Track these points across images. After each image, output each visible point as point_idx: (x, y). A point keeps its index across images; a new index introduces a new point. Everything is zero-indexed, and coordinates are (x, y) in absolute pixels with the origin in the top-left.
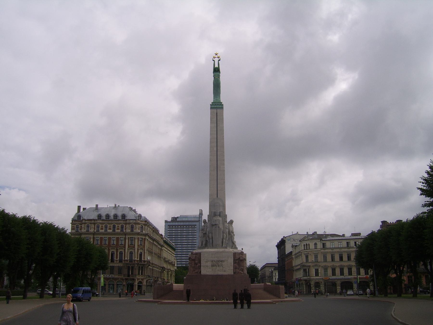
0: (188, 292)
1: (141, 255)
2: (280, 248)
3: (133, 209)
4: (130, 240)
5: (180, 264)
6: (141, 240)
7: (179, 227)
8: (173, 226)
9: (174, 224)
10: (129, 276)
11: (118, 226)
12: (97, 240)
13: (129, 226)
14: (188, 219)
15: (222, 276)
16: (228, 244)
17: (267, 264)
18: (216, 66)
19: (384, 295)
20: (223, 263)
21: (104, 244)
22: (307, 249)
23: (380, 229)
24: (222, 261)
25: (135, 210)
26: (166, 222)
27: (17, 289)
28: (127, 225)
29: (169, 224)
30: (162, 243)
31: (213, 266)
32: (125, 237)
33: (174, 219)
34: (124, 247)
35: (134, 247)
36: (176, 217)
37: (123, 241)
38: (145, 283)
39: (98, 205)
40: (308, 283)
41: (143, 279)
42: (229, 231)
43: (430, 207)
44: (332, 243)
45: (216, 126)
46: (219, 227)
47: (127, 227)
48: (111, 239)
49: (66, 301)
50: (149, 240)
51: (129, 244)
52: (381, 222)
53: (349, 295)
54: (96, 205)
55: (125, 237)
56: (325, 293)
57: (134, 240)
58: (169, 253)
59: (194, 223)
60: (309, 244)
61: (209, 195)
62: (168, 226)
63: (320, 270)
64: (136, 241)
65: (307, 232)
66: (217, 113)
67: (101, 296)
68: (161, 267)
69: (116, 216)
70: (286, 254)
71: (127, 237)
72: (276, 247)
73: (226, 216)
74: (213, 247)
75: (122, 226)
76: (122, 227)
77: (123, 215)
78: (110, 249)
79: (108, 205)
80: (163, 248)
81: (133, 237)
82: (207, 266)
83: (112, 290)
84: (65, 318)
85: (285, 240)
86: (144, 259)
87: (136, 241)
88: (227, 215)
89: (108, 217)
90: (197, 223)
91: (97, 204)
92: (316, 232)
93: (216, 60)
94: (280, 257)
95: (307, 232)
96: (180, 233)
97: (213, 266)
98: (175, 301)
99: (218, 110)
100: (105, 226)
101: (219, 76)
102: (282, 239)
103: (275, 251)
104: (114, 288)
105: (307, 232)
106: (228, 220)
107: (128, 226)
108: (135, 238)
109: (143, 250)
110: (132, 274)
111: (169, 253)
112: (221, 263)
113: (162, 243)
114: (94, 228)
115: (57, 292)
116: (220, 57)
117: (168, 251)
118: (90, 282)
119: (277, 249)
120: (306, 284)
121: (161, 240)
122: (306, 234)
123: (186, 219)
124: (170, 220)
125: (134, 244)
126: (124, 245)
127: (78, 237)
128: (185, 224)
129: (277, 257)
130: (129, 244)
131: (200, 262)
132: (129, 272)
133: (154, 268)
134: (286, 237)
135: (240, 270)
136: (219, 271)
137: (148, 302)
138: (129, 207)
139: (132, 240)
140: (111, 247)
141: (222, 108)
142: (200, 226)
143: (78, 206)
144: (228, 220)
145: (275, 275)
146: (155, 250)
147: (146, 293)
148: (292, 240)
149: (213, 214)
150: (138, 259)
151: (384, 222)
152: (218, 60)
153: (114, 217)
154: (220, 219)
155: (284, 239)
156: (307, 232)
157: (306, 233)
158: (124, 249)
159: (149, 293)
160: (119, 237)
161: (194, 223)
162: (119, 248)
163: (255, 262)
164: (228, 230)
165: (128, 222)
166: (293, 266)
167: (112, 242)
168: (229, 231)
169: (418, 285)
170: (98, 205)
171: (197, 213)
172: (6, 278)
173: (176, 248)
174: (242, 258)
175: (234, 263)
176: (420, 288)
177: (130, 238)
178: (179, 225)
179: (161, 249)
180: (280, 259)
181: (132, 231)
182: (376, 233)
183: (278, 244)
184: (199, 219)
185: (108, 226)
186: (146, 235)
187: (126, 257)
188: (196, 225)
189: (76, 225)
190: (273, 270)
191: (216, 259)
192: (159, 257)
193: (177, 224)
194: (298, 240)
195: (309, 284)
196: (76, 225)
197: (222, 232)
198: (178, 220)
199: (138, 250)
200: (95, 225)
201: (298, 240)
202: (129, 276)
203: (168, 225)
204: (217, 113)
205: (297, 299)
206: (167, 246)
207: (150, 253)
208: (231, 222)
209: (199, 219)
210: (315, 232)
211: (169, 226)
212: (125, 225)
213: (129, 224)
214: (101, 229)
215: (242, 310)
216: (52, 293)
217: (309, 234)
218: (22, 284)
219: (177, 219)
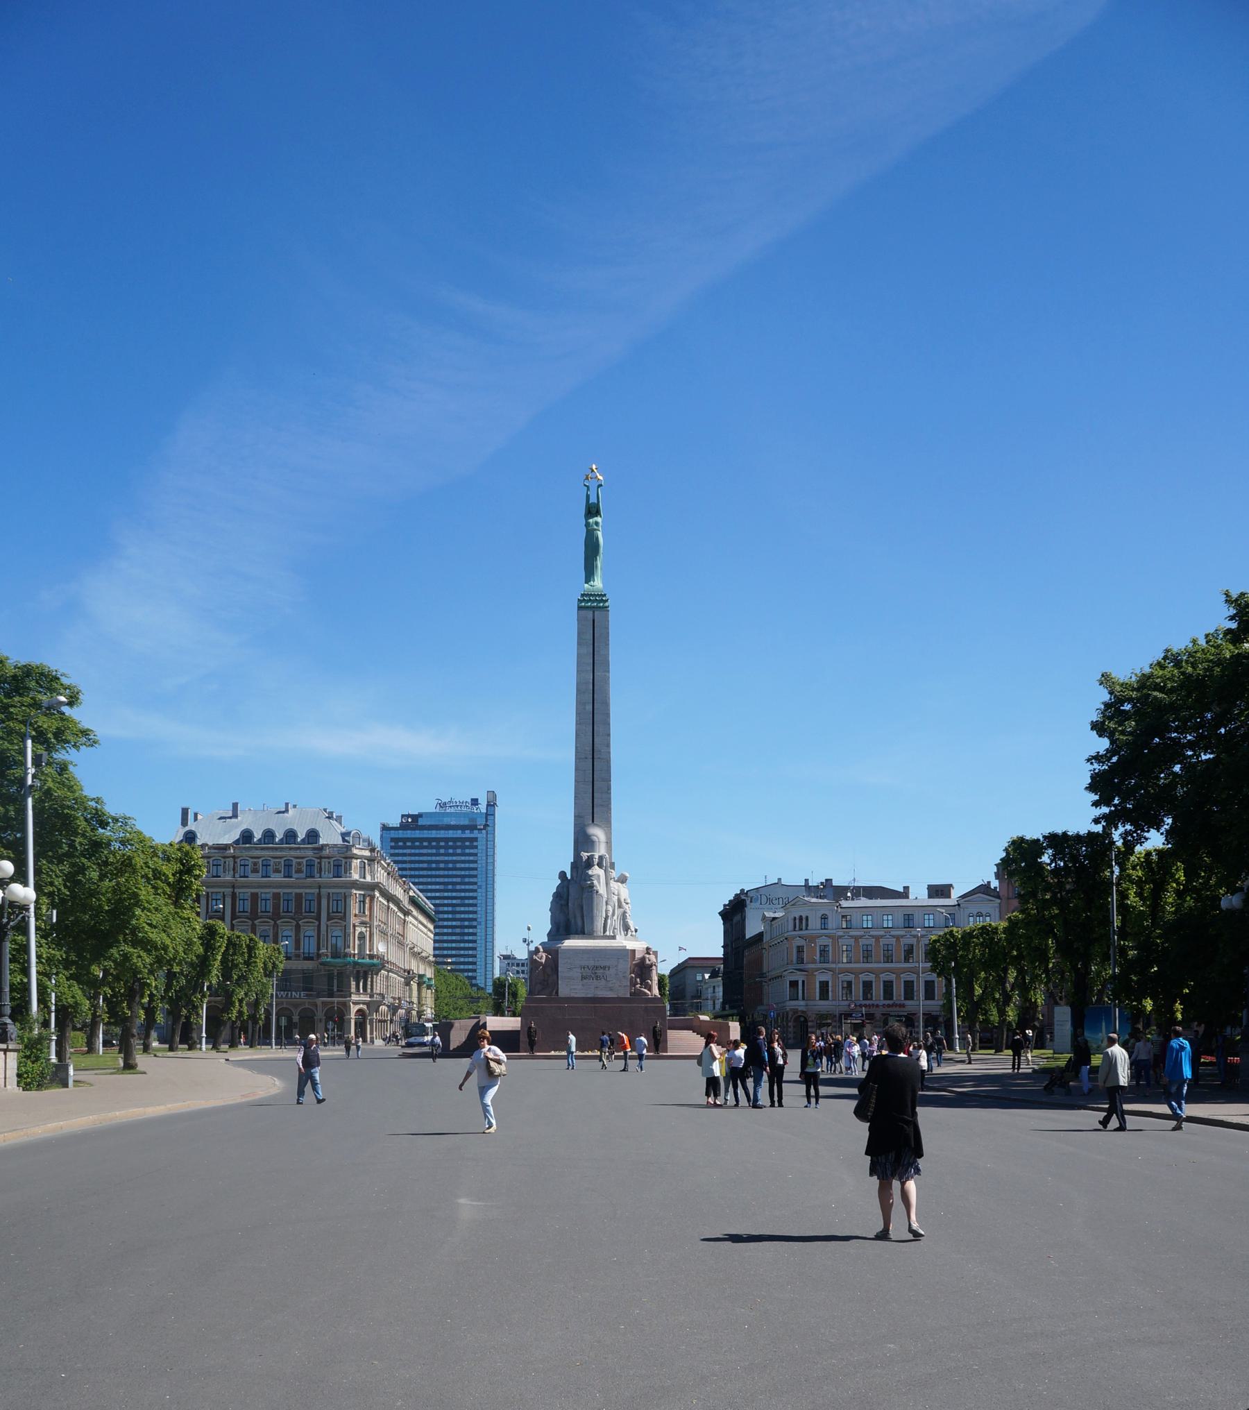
0: (530, 1033)
2: (732, 920)
3: (322, 841)
4: (210, 899)
5: (469, 934)
6: (362, 900)
8: (405, 840)
9: (409, 834)
11: (299, 864)
12: (216, 899)
13: (329, 863)
14: (390, 834)
17: (690, 958)
18: (593, 500)
19: (375, 976)
20: (607, 972)
21: (307, 910)
22: (801, 929)
24: (604, 968)
25: (999, 863)
26: (385, 828)
27: (224, 929)
28: (323, 860)
29: (394, 834)
30: (406, 903)
31: (583, 978)
32: (319, 894)
33: (412, 822)
34: (316, 920)
36: (417, 813)
37: (268, 901)
39: (908, 887)
40: (801, 1016)
42: (619, 900)
44: (867, 915)
45: (595, 737)
47: (323, 867)
48: (302, 898)
50: (398, 914)
51: (331, 911)
52: (783, 1104)
54: (233, 804)
55: (319, 894)
57: (343, 900)
58: (422, 932)
60: (807, 918)
61: (123, 1075)
62: (391, 842)
63: (787, 991)
65: (807, 880)
66: (1141, 1130)
68: (405, 971)
69: (291, 835)
70: (747, 937)
72: (720, 917)
75: (336, 863)
77: (313, 834)
78: (255, 925)
79: (264, 805)
80: (1052, 999)
81: (291, 893)
85: (744, 900)
88: (996, 879)
91: (234, 802)
92: (831, 880)
94: (729, 943)
95: (806, 880)
96: (452, 885)
97: (583, 978)
98: (255, 1057)
100: (215, 864)
102: (736, 895)
103: (716, 930)
104: (611, 850)
105: (806, 880)
107: (327, 863)
108: (224, 895)
109: (366, 927)
111: (422, 932)
112: (602, 971)
114: (234, 870)
115: (1104, 1024)
117: (420, 926)
118: (1202, 1060)
119: (722, 922)
121: (388, 879)
122: (803, 884)
125: (343, 911)
126: (271, 914)
127: (1161, 700)
128: (451, 834)
129: (722, 945)
130: (331, 911)
133: (390, 974)
134: (747, 891)
138: (613, 861)
140: (282, 918)
145: (714, 1002)
147: (376, 1039)
148: (764, 899)
149: (497, 1075)
150: (354, 950)
151: (1089, 831)
152: (597, 485)
153: (310, 838)
155: (743, 897)
156: (807, 880)
157: (804, 881)
158: (317, 923)
159: (475, 971)
160: (280, 893)
162: (303, 921)
163: (221, 818)
164: (616, 897)
167: (261, 906)
168: (619, 900)
170: (908, 887)
172: (1185, 1092)
173: (379, 978)
174: (649, 961)
176: (1191, 675)
177: (210, 894)
179: (405, 920)
180: (730, 949)
182: (1122, 796)
183: (725, 909)
184: (486, 821)
185: (294, 864)
187: (323, 946)
188: (476, 839)
189: (307, 861)
193: (418, 834)
194: (781, 899)
195: (802, 1019)
196: (285, 861)
197: (604, 903)
198: (421, 822)
200: (236, 860)
201: (781, 899)
203: (391, 838)
204: (1141, 1130)
206: (597, 918)
209: (486, 821)
210: (827, 880)
211: (393, 840)
212: (319, 860)
213: (328, 858)
214: (296, 872)
216: (1122, 1083)
217: (810, 885)
219: (420, 819)
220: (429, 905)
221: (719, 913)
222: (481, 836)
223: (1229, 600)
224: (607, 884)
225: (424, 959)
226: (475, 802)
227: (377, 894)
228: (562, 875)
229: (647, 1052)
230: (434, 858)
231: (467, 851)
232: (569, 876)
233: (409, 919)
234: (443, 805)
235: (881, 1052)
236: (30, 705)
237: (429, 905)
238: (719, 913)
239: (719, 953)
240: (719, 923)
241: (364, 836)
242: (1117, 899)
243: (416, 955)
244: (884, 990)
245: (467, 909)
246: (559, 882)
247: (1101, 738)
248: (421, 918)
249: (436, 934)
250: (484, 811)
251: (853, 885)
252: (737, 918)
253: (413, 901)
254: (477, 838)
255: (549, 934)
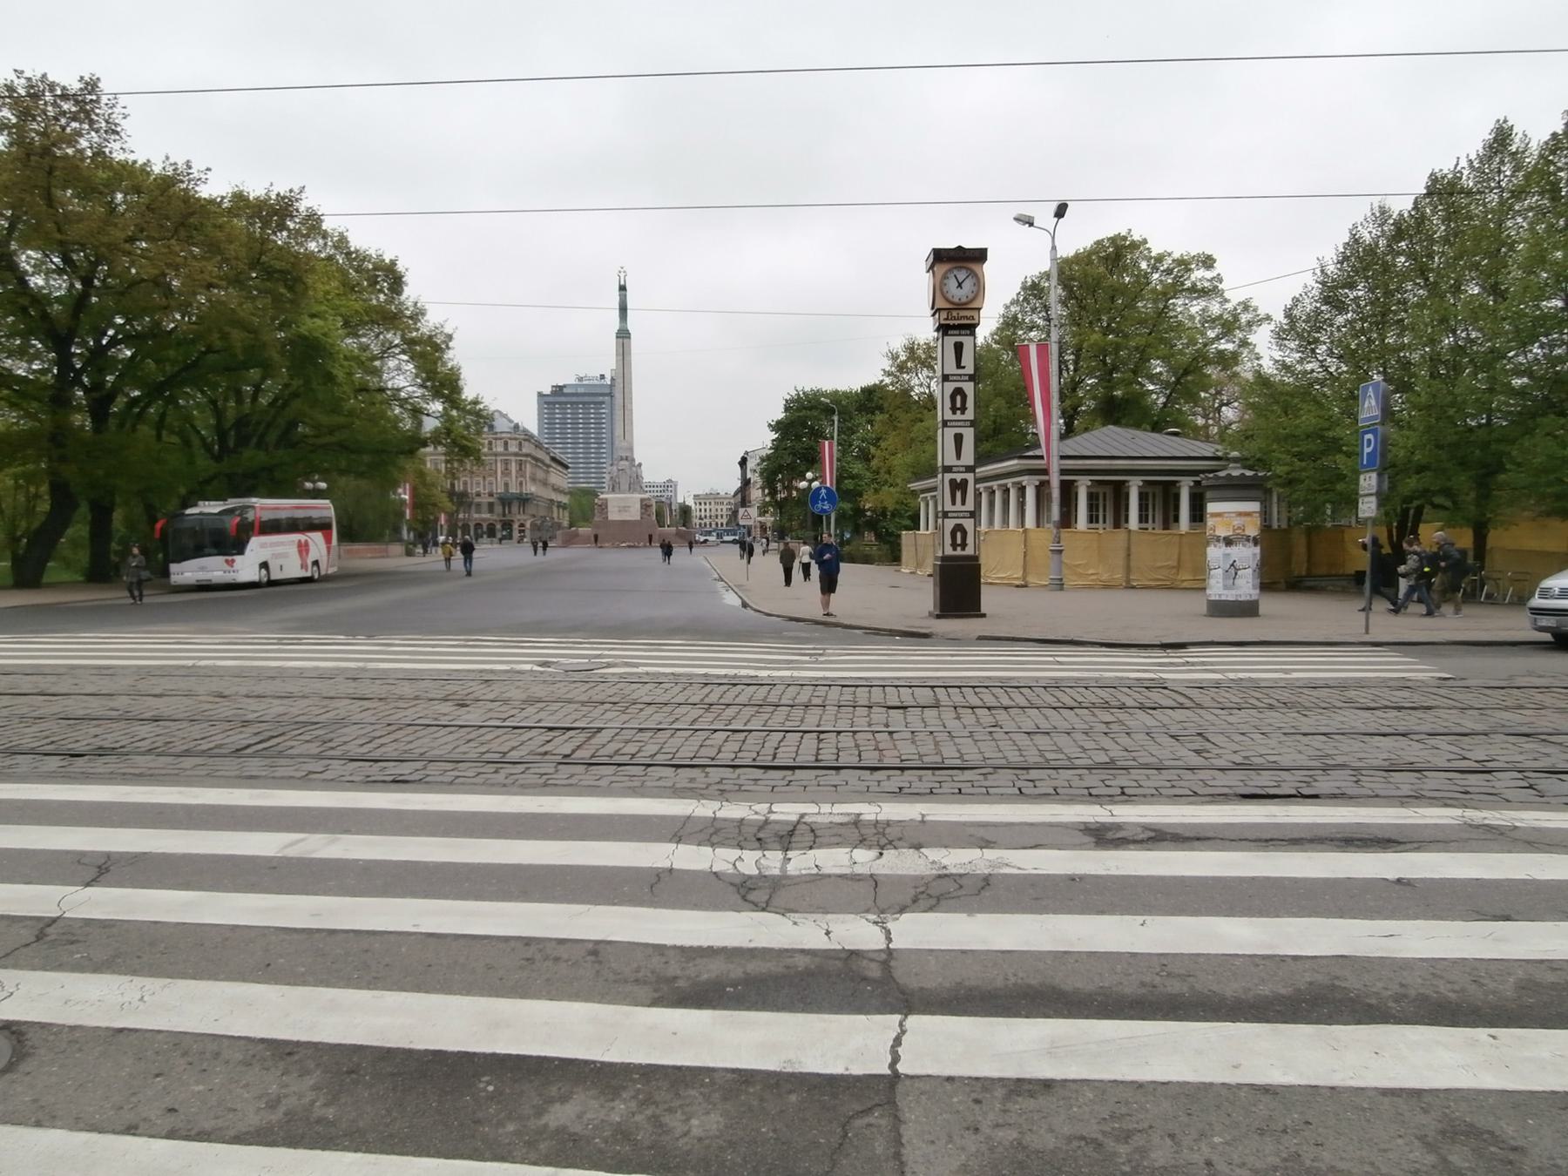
1: (521, 484)
8: (554, 403)
10: (504, 515)
16: (960, 790)
18: (622, 283)
26: (540, 395)
30: (548, 461)
33: (558, 390)
35: (510, 473)
38: (528, 525)
41: (525, 520)
43: (1059, 307)
46: (1032, 885)
49: (565, 494)
59: (601, 399)
64: (513, 464)
66: (623, 335)
67: (487, 516)
71: (499, 458)
73: (633, 460)
74: (620, 492)
76: (490, 443)
87: (513, 464)
89: (867, 703)
90: (607, 399)
93: (622, 275)
99: (914, 1021)
101: (625, 296)
102: (834, 591)
106: (637, 463)
110: (510, 512)
113: (548, 461)
116: (1253, 303)
120: (761, 527)
124: (547, 391)
129: (780, 415)
132: (504, 511)
137: (70, 777)
139: (506, 463)
141: (629, 338)
143: (941, 257)
144: (637, 463)
146: (540, 474)
161: (601, 399)
164: (729, 1075)
165: (499, 436)
166: (889, 1072)
169: (1402, 546)
175: (641, 508)
178: (581, 403)
181: (491, 449)
186: (527, 455)
188: (603, 403)
192: (545, 483)
193: (563, 399)
198: (565, 390)
202: (504, 515)
207: (533, 479)
208: (640, 465)
215: (1063, 197)
218: (83, 426)
221: (986, 249)
226: (602, 377)
234: (581, 379)
235: (1369, 467)
236: (97, 386)
238: (986, 249)
241: (1008, 302)
247: (1208, 252)
250: (609, 383)
251: (1221, 580)
254: (1380, 207)
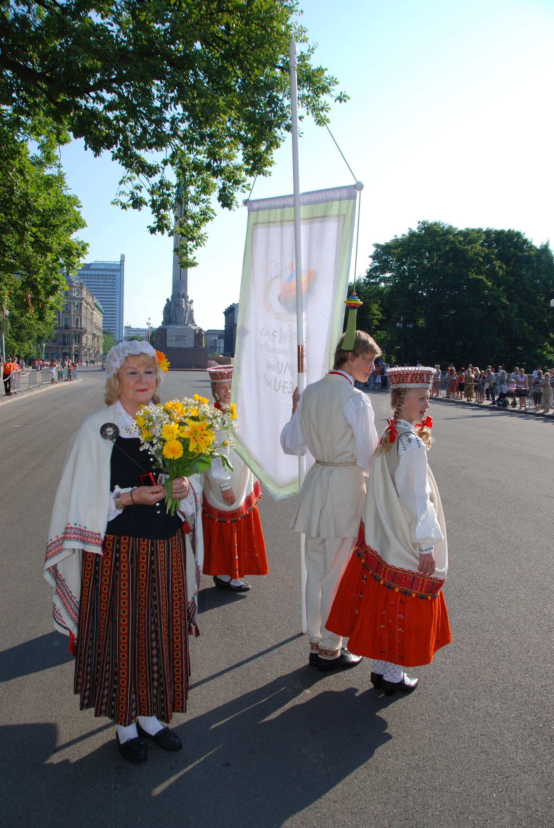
7: (93, 277)
8: (84, 275)
9: (86, 272)
15: (192, 721)
23: (203, 333)
24: (184, 336)
25: (83, 698)
28: (160, 475)
53: (195, 540)
56: (378, 328)
73: (188, 297)
82: (172, 340)
83: (168, 508)
84: (249, 135)
86: (81, 326)
97: (176, 340)
106: (189, 300)
123: (103, 267)
128: (100, 273)
131: (166, 336)
135: (399, 383)
136: (181, 345)
142: (279, 211)
154: (428, 432)
171: (118, 260)
188: (115, 276)
190: (216, 338)
191: (179, 334)
193: (89, 272)
198: (91, 267)
199: (74, 316)
205: (142, 469)
208: (192, 302)
220: (101, 307)
222: (118, 274)
223: (370, 257)
224: (186, 304)
225: (99, 329)
227: (83, 302)
228: (168, 300)
229: (75, 348)
230: (89, 280)
231: (108, 280)
232: (170, 300)
233: (94, 312)
237: (101, 307)
239: (223, 329)
240: (224, 316)
242: (191, 763)
243: (96, 327)
244: (442, 500)
245: (111, 306)
246: (166, 302)
248: (98, 312)
249: (104, 317)
252: (231, 315)
253: (95, 304)
255: (163, 323)
